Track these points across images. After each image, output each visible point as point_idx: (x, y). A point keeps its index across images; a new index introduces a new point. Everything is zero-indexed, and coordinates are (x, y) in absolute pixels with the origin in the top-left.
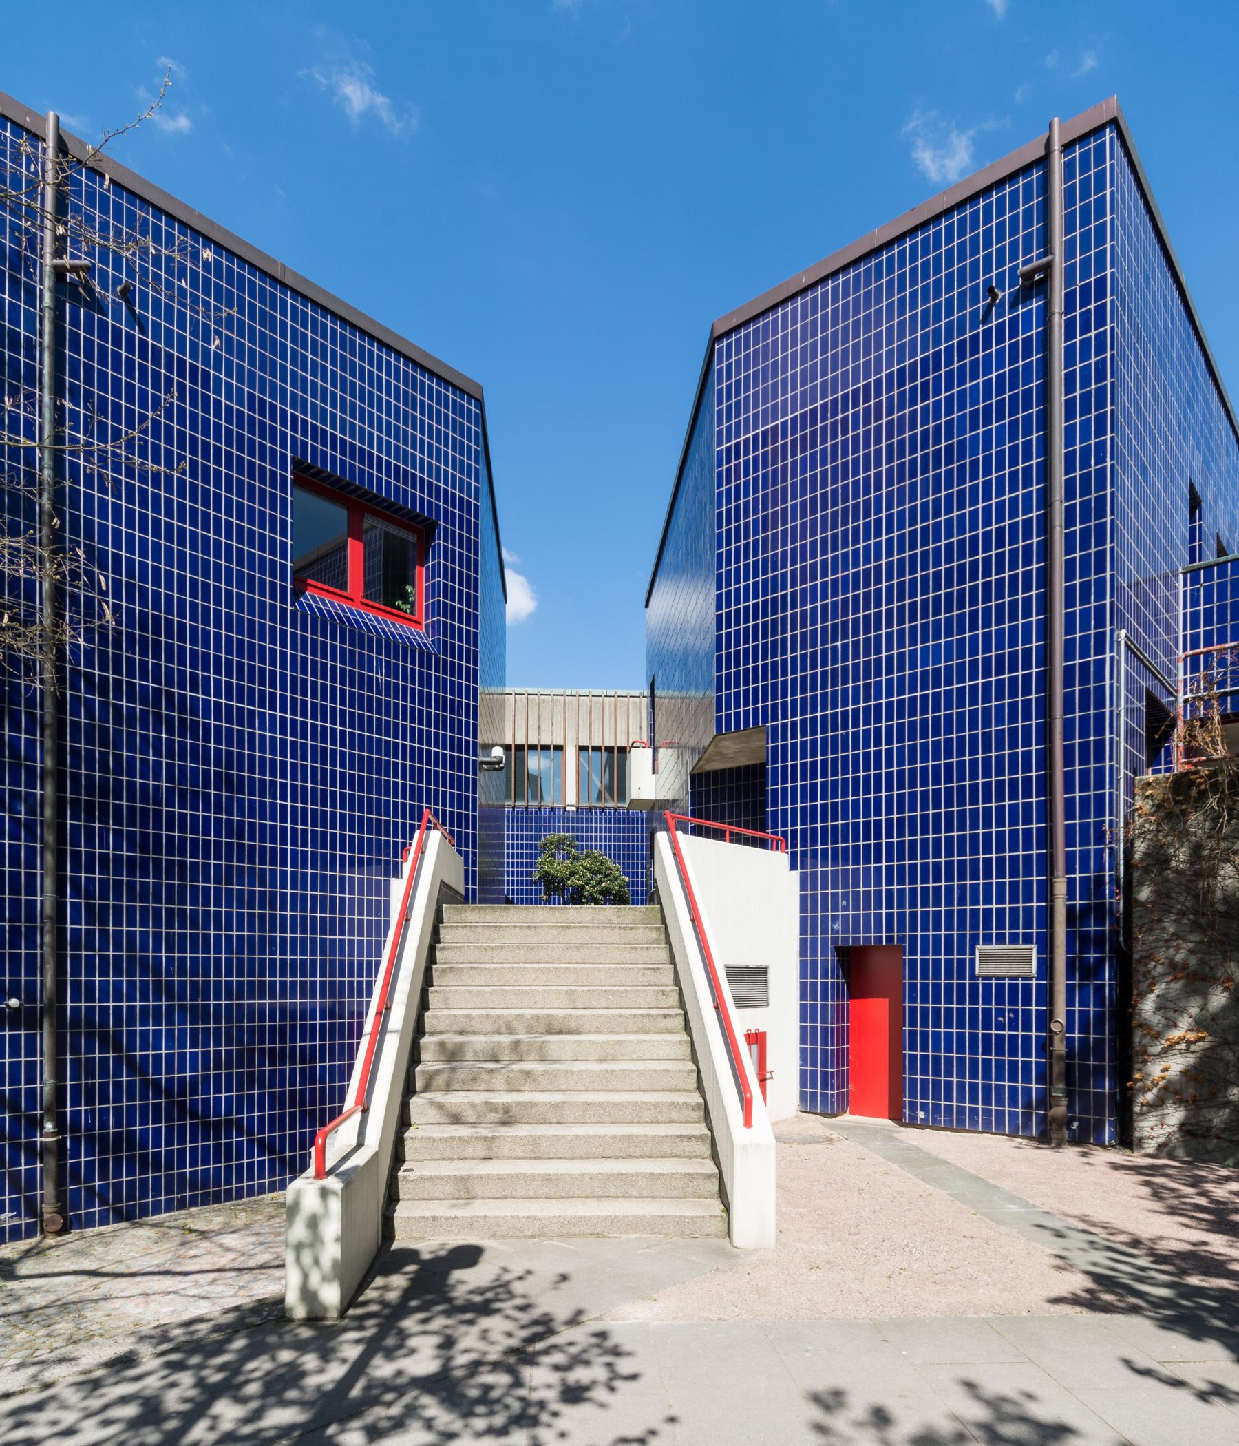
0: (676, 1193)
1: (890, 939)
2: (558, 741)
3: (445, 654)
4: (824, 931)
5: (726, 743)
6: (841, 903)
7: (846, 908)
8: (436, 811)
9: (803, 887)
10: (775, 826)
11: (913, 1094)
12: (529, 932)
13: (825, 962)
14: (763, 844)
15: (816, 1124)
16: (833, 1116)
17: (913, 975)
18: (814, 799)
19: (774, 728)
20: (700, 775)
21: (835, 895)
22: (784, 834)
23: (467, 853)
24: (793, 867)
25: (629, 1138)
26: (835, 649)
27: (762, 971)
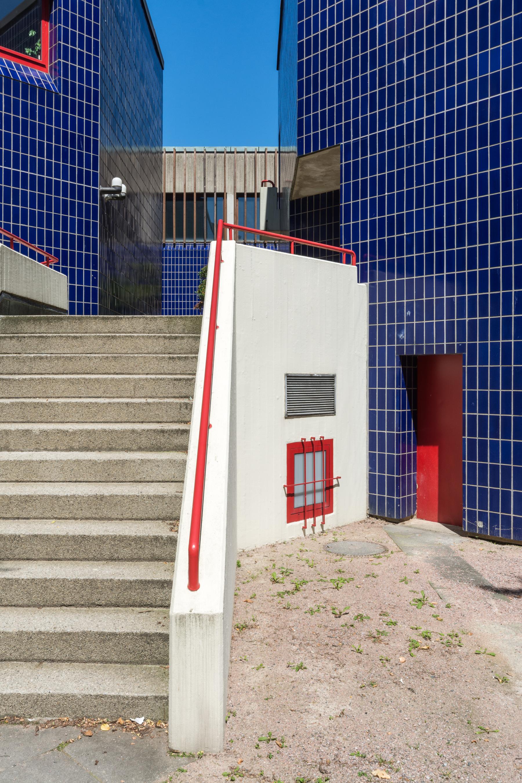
0: (130, 657)
1: (450, 348)
2: (220, 190)
3: (66, 92)
4: (391, 341)
5: (310, 166)
6: (407, 313)
7: (410, 318)
8: (16, 228)
9: (372, 298)
10: (347, 241)
11: (472, 504)
12: (75, 342)
13: (391, 371)
14: (336, 257)
15: (381, 531)
16: (396, 522)
17: (472, 385)
18: (382, 213)
19: (347, 146)
20: (298, 200)
21: (400, 306)
22: (355, 247)
23: (72, 271)
24: (362, 278)
25: (92, 583)
26: (400, 64)
27: (329, 380)
